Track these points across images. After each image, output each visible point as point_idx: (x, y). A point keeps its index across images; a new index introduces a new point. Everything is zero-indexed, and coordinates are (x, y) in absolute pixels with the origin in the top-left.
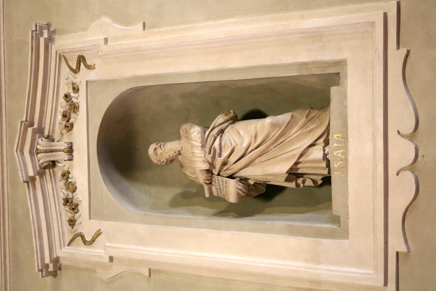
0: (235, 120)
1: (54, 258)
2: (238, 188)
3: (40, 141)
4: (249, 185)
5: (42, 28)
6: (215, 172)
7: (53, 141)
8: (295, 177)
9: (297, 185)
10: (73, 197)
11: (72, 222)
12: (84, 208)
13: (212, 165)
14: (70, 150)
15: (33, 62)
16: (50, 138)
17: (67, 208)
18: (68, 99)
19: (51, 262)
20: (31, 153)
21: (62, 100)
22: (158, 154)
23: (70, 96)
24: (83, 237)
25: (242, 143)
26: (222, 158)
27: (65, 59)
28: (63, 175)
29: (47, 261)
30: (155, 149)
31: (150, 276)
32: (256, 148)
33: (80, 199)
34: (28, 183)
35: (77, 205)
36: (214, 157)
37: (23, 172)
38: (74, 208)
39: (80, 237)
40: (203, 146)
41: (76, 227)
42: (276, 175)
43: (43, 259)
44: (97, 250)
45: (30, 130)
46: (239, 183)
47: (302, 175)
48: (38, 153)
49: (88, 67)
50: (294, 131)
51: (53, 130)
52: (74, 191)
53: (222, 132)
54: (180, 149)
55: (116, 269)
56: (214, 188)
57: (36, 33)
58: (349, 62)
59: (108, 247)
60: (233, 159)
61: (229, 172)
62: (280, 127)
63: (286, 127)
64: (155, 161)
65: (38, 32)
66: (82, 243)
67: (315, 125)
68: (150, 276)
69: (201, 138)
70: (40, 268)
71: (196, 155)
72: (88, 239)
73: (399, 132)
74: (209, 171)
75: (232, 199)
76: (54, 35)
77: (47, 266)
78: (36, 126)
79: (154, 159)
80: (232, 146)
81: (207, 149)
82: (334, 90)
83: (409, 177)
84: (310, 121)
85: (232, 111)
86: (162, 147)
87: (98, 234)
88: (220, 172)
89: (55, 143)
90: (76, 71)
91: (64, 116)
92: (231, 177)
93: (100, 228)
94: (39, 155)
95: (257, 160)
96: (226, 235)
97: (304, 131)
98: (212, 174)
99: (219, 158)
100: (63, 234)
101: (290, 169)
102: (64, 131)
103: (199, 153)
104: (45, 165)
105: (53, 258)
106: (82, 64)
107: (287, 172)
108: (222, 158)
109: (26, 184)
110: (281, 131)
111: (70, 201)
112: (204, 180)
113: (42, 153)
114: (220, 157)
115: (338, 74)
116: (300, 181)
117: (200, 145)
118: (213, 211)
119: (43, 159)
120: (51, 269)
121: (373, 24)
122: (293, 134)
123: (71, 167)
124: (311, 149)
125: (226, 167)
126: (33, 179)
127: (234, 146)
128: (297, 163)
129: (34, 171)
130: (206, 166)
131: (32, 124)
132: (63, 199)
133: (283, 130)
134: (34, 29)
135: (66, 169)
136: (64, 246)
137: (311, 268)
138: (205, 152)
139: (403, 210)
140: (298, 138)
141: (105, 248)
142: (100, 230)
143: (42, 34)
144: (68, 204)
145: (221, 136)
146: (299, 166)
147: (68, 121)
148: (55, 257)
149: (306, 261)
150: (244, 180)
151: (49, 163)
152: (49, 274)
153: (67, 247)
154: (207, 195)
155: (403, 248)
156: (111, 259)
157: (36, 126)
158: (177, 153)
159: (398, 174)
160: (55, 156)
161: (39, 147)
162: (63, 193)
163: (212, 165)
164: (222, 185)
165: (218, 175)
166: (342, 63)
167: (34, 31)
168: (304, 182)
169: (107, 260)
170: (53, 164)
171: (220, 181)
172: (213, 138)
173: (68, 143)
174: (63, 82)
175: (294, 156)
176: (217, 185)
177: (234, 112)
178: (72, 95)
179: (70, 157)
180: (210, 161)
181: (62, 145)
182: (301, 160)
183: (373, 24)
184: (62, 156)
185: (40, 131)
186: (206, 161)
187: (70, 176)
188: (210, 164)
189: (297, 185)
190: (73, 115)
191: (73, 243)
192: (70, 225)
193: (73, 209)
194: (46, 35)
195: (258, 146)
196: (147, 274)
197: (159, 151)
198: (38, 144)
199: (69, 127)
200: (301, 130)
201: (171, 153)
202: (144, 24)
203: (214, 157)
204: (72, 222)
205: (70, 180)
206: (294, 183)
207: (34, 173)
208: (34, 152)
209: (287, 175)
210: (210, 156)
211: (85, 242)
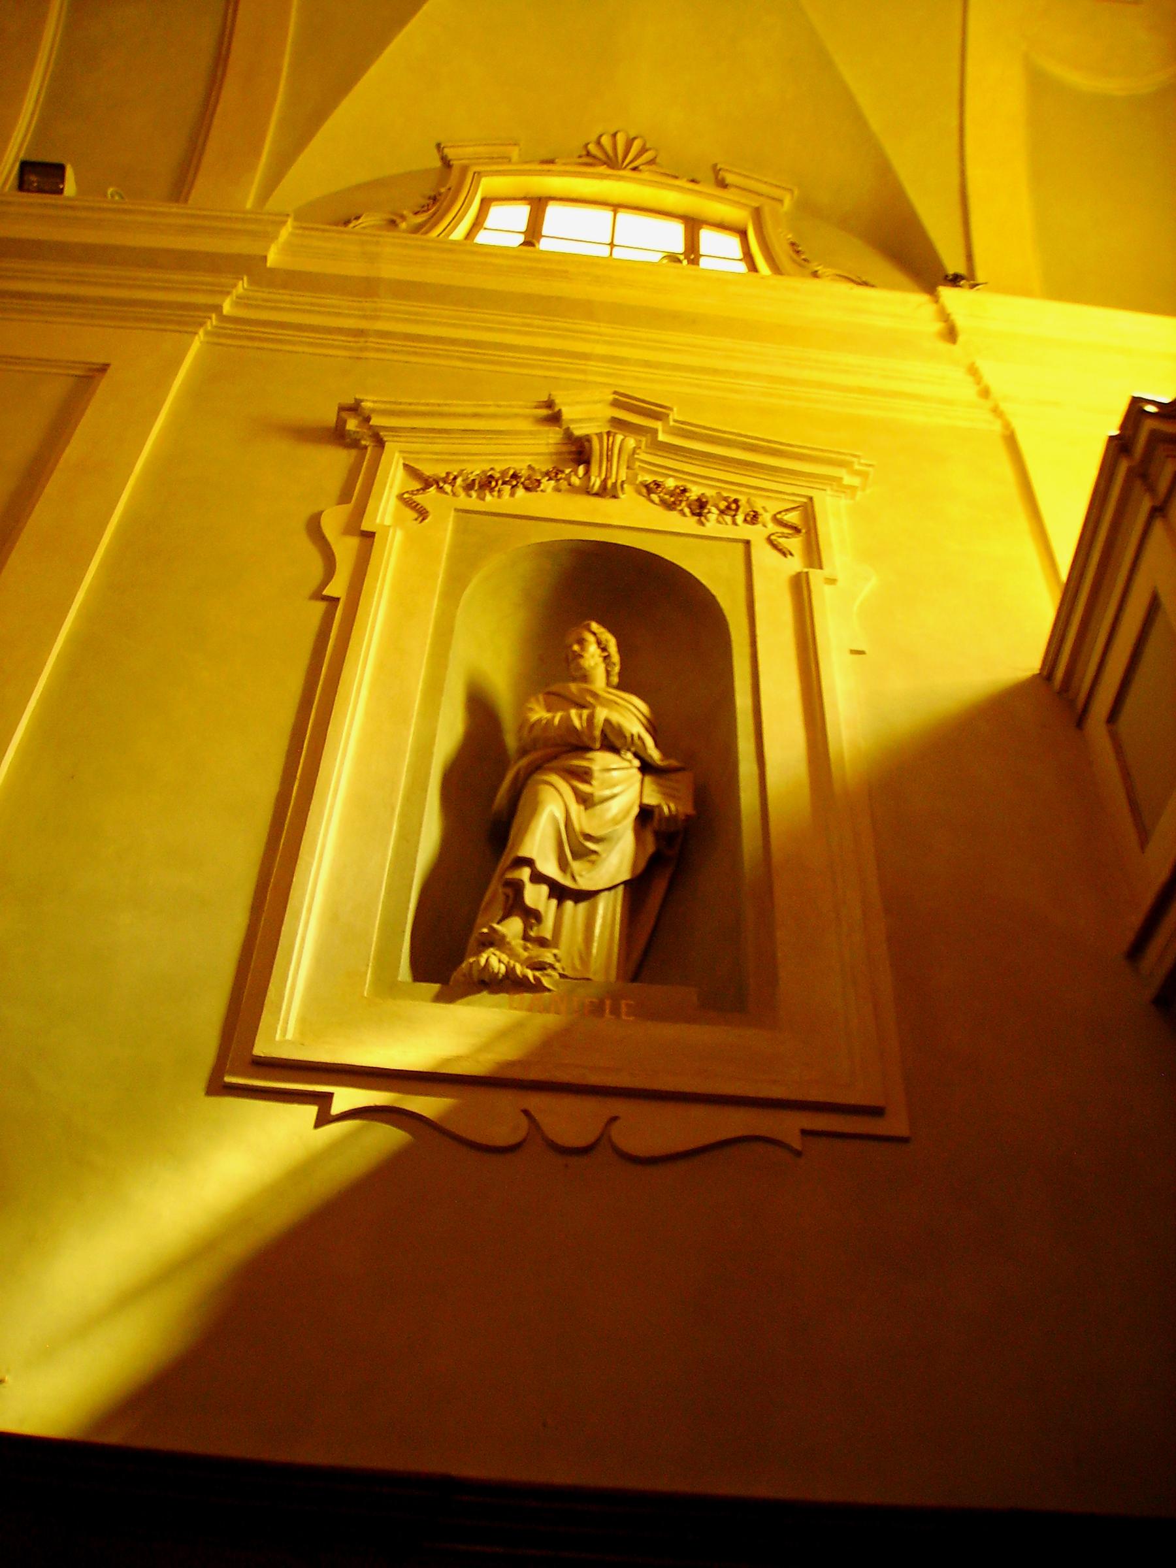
14: (607, 491)
48: (608, 433)
55: (345, 549)
73: (614, 1119)
126: (555, 419)
136: (404, 458)
148: (385, 439)
153: (401, 462)
155: (337, 1108)
156: (370, 535)
159: (526, 1112)
169: (366, 526)
196: (326, 592)
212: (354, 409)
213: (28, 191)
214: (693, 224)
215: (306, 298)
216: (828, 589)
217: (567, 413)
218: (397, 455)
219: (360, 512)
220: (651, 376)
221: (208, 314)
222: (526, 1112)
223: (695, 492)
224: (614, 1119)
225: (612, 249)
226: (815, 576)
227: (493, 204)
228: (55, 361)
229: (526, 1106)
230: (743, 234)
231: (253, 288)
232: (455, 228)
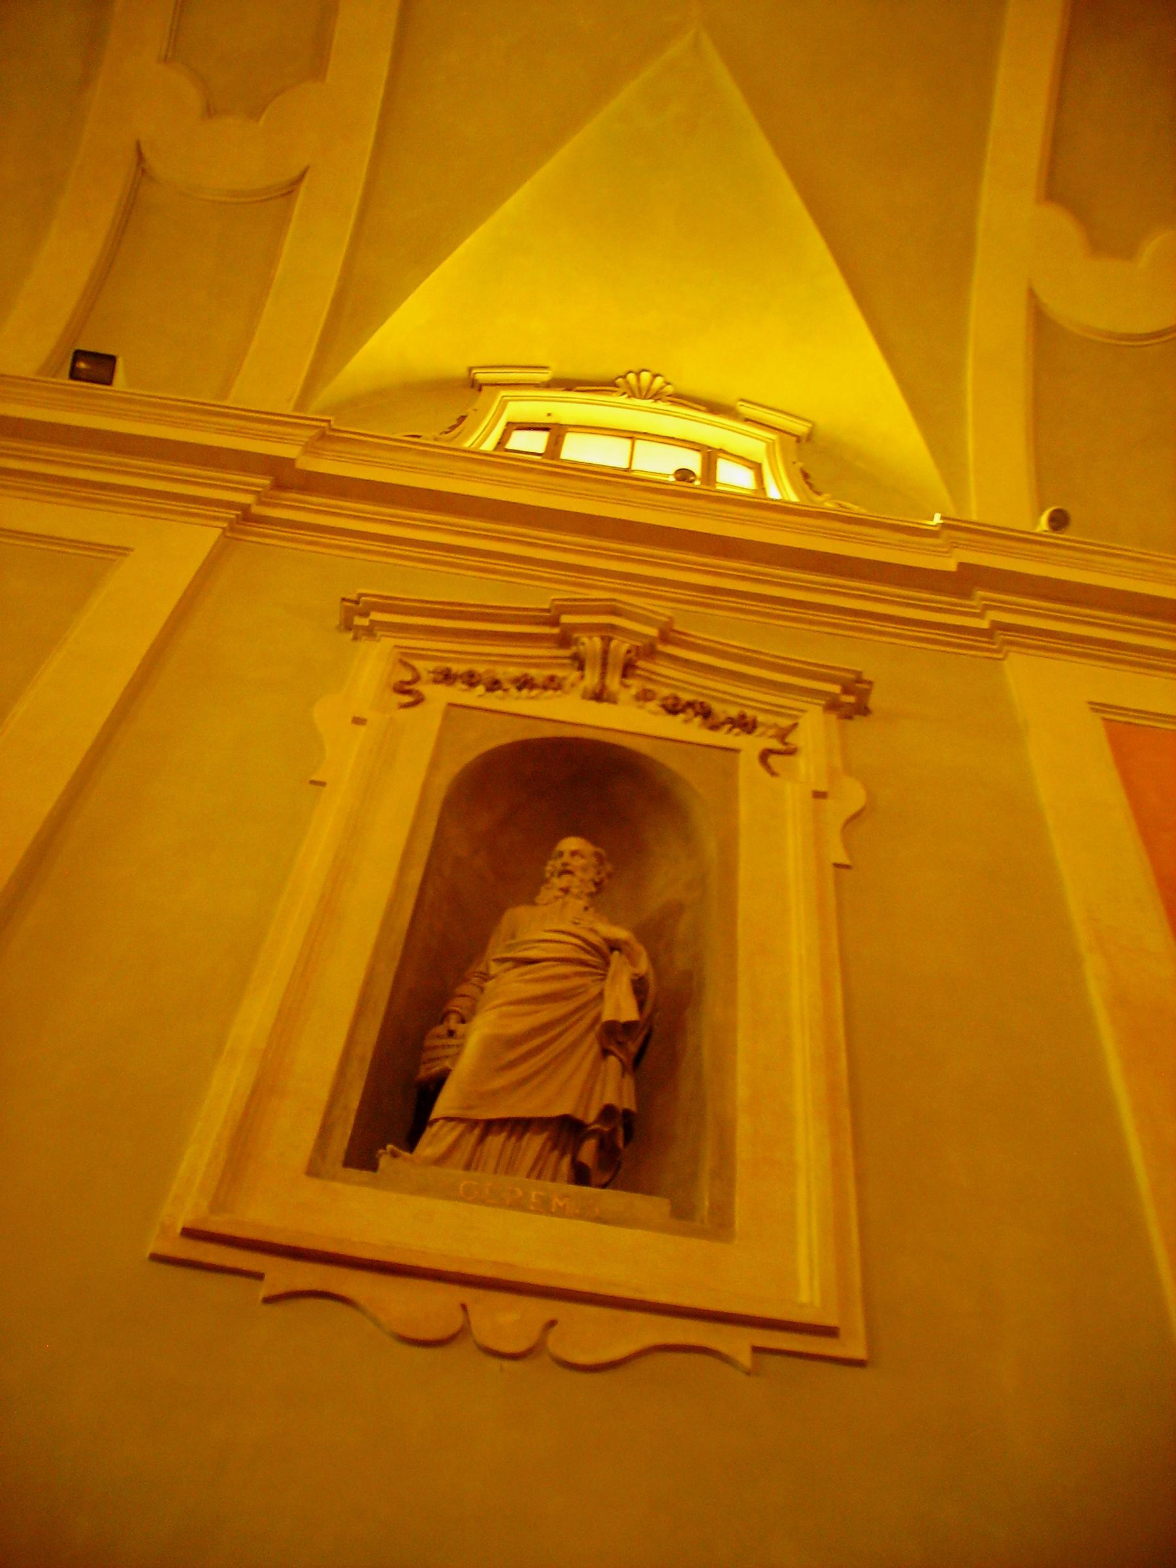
14: (599, 695)
73: (552, 1323)
159: (464, 1307)
212: (344, 599)
224: (552, 1323)
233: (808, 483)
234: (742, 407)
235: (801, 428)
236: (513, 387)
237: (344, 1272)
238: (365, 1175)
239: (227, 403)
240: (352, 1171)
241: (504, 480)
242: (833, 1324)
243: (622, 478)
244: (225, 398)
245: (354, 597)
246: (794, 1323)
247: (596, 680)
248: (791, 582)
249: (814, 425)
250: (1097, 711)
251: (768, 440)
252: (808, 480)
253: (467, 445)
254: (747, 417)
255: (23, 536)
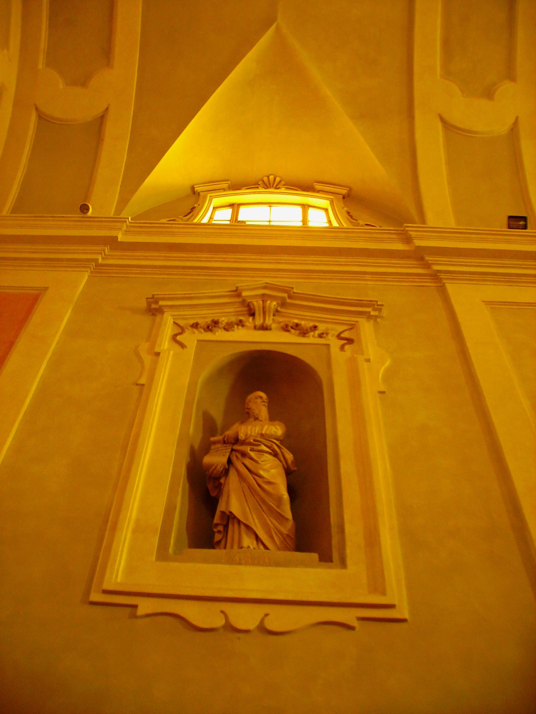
0: (288, 472)
1: (163, 309)
2: (217, 465)
3: (275, 303)
4: (220, 478)
5: (380, 310)
6: (236, 447)
7: (274, 315)
8: (225, 523)
9: (217, 525)
10: (220, 328)
11: (195, 326)
12: (208, 336)
13: (244, 443)
14: (264, 328)
15: (349, 301)
16: (277, 312)
17: (209, 322)
18: (312, 328)
19: (161, 306)
20: (263, 295)
21: (311, 324)
22: (256, 400)
23: (315, 330)
24: (180, 334)
25: (264, 470)
26: (249, 452)
27: (351, 329)
28: (241, 321)
29: (161, 303)
30: (261, 397)
31: (137, 384)
32: (257, 484)
33: (217, 334)
34: (236, 291)
35: (211, 330)
36: (250, 444)
37: (246, 287)
38: (208, 328)
39: (181, 331)
40: (262, 435)
41: (190, 328)
42: (228, 503)
43: (163, 299)
44: (167, 343)
45: (286, 295)
46: (223, 467)
47: (226, 527)
48: (263, 301)
49: (342, 348)
50: (272, 522)
51: (283, 316)
52: (225, 329)
53: (275, 455)
54: (260, 419)
55: (147, 359)
56: (219, 445)
57: (374, 304)
58: (344, 571)
59: (169, 353)
60: (247, 462)
61: (234, 459)
62: (278, 507)
63: (278, 512)
64: (249, 397)
65: (376, 306)
66: (175, 333)
67: (278, 543)
68: (137, 384)
69: (269, 433)
70: (156, 296)
71: (254, 428)
72: (178, 338)
73: (267, 615)
74: (237, 440)
75: (207, 460)
76: (373, 321)
77: (157, 302)
78: (288, 301)
79: (251, 397)
80: (260, 461)
81: (259, 439)
82: (315, 556)
83: (220, 622)
84: (284, 538)
85: (295, 469)
86: (263, 403)
87: (182, 346)
88: (236, 451)
89: (272, 317)
90: (339, 337)
91: (297, 325)
92: (229, 461)
93: (188, 348)
94: (261, 302)
95: (245, 485)
96: (172, 451)
97: (273, 531)
98: (234, 444)
99: (249, 449)
100: (185, 319)
101: (233, 516)
102: (282, 324)
103: (255, 430)
104: (252, 306)
105: (163, 308)
106: (345, 342)
107: (231, 512)
108: (249, 452)
109: (234, 289)
110: (274, 506)
111: (216, 325)
112: (228, 435)
113: (263, 304)
114: (250, 450)
115: (332, 561)
116: (221, 528)
117: (263, 432)
118: (196, 446)
119: (257, 304)
120: (153, 306)
121: (384, 593)
122: (270, 520)
123: (248, 328)
124: (253, 537)
125: (239, 456)
126: (239, 295)
127: (260, 464)
128: (239, 522)
129: (246, 296)
130: (242, 436)
131: (290, 297)
132: (218, 320)
133: (275, 509)
134: (379, 303)
135: (247, 324)
136: (173, 319)
137: (129, 523)
138: (256, 437)
139: (182, 614)
140: (265, 525)
141: (169, 350)
142: (186, 347)
143: (375, 310)
144: (213, 324)
145: (270, 454)
146: (236, 526)
147: (292, 328)
148: (165, 310)
149: (138, 520)
150: (226, 472)
151: (253, 310)
152: (149, 304)
153: (172, 321)
154: (212, 439)
155: (141, 611)
156: (158, 354)
157: (288, 301)
158: (256, 416)
159: (222, 612)
160: (260, 315)
161: (269, 302)
162: (224, 320)
163: (244, 443)
164: (222, 453)
165: (232, 450)
166: (343, 564)
167: (377, 303)
168: (219, 532)
169: (157, 350)
170: (253, 314)
171: (226, 451)
172: (269, 445)
173: (270, 326)
174: (330, 326)
175: (247, 519)
176: (222, 449)
177: (295, 471)
178: (317, 332)
179: (257, 327)
180: (248, 441)
181: (269, 321)
182: (242, 527)
183: (384, 593)
184: (259, 321)
185: (283, 304)
186: (247, 437)
187: (240, 327)
188: (244, 440)
189: (217, 525)
190: (298, 332)
191: (176, 326)
192: (193, 324)
193: (208, 327)
194: (372, 313)
195: (259, 485)
197: (259, 400)
198: (271, 302)
199: (286, 328)
200: (274, 527)
201: (256, 411)
202: (383, 392)
203: (250, 444)
204: (195, 326)
205: (236, 326)
206: (219, 522)
207: (245, 296)
208: (264, 297)
209: (228, 513)
210: (252, 441)
211: (176, 335)
212: (147, 298)
213: (509, 221)
214: (305, 207)
215: (231, 256)
216: (365, 364)
217: (244, 294)
218: (170, 317)
219: (154, 344)
220: (131, 271)
221: (92, 263)
222: (222, 612)
223: (322, 327)
224: (267, 615)
225: (268, 221)
226: (360, 359)
227: (241, 207)
228: (3, 286)
229: (223, 609)
230: (326, 210)
231: (111, 251)
232: (203, 218)
233: (350, 216)
234: (316, 186)
235: (344, 192)
236: (325, 193)
237: (172, 601)
238: (330, 564)
239: (121, 216)
240: (323, 563)
241: (245, 235)
242: (259, 597)
243: (417, 228)
244: (119, 215)
245: (151, 296)
246: (377, 604)
247: (262, 321)
248: (380, 265)
249: (351, 189)
250: (487, 304)
251: (330, 199)
252: (350, 214)
253: (195, 221)
254: (319, 189)
255: (12, 288)
